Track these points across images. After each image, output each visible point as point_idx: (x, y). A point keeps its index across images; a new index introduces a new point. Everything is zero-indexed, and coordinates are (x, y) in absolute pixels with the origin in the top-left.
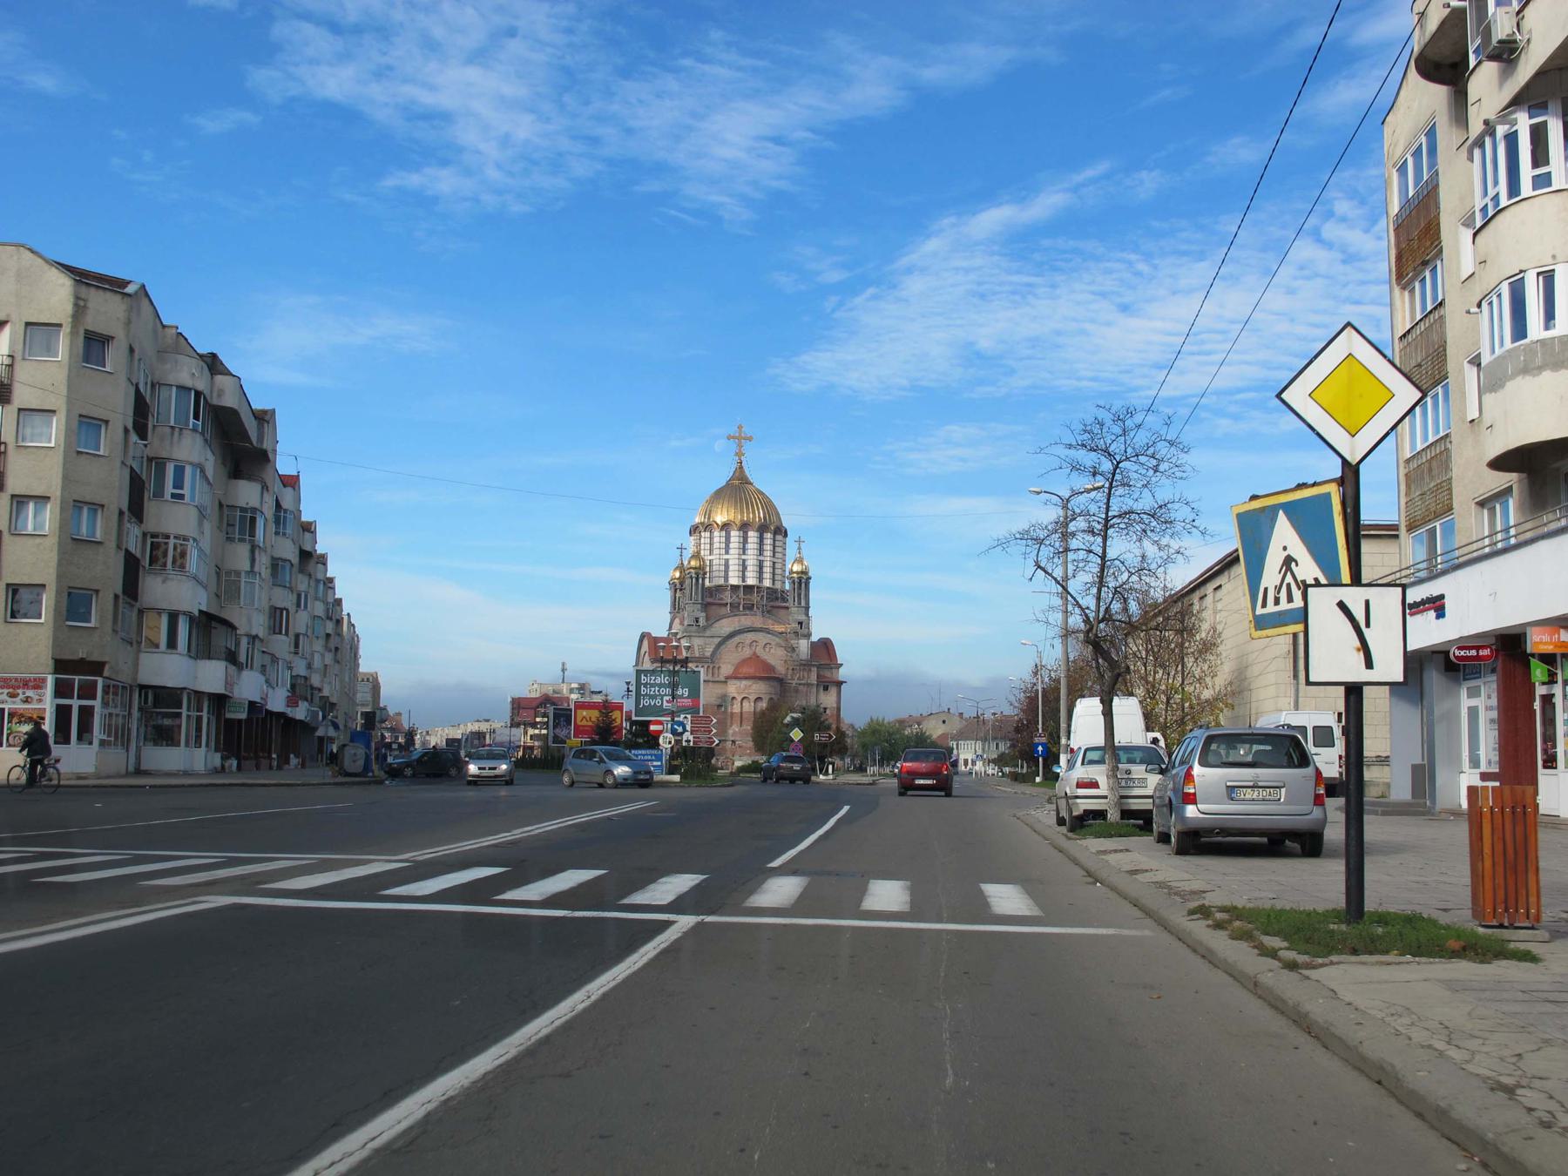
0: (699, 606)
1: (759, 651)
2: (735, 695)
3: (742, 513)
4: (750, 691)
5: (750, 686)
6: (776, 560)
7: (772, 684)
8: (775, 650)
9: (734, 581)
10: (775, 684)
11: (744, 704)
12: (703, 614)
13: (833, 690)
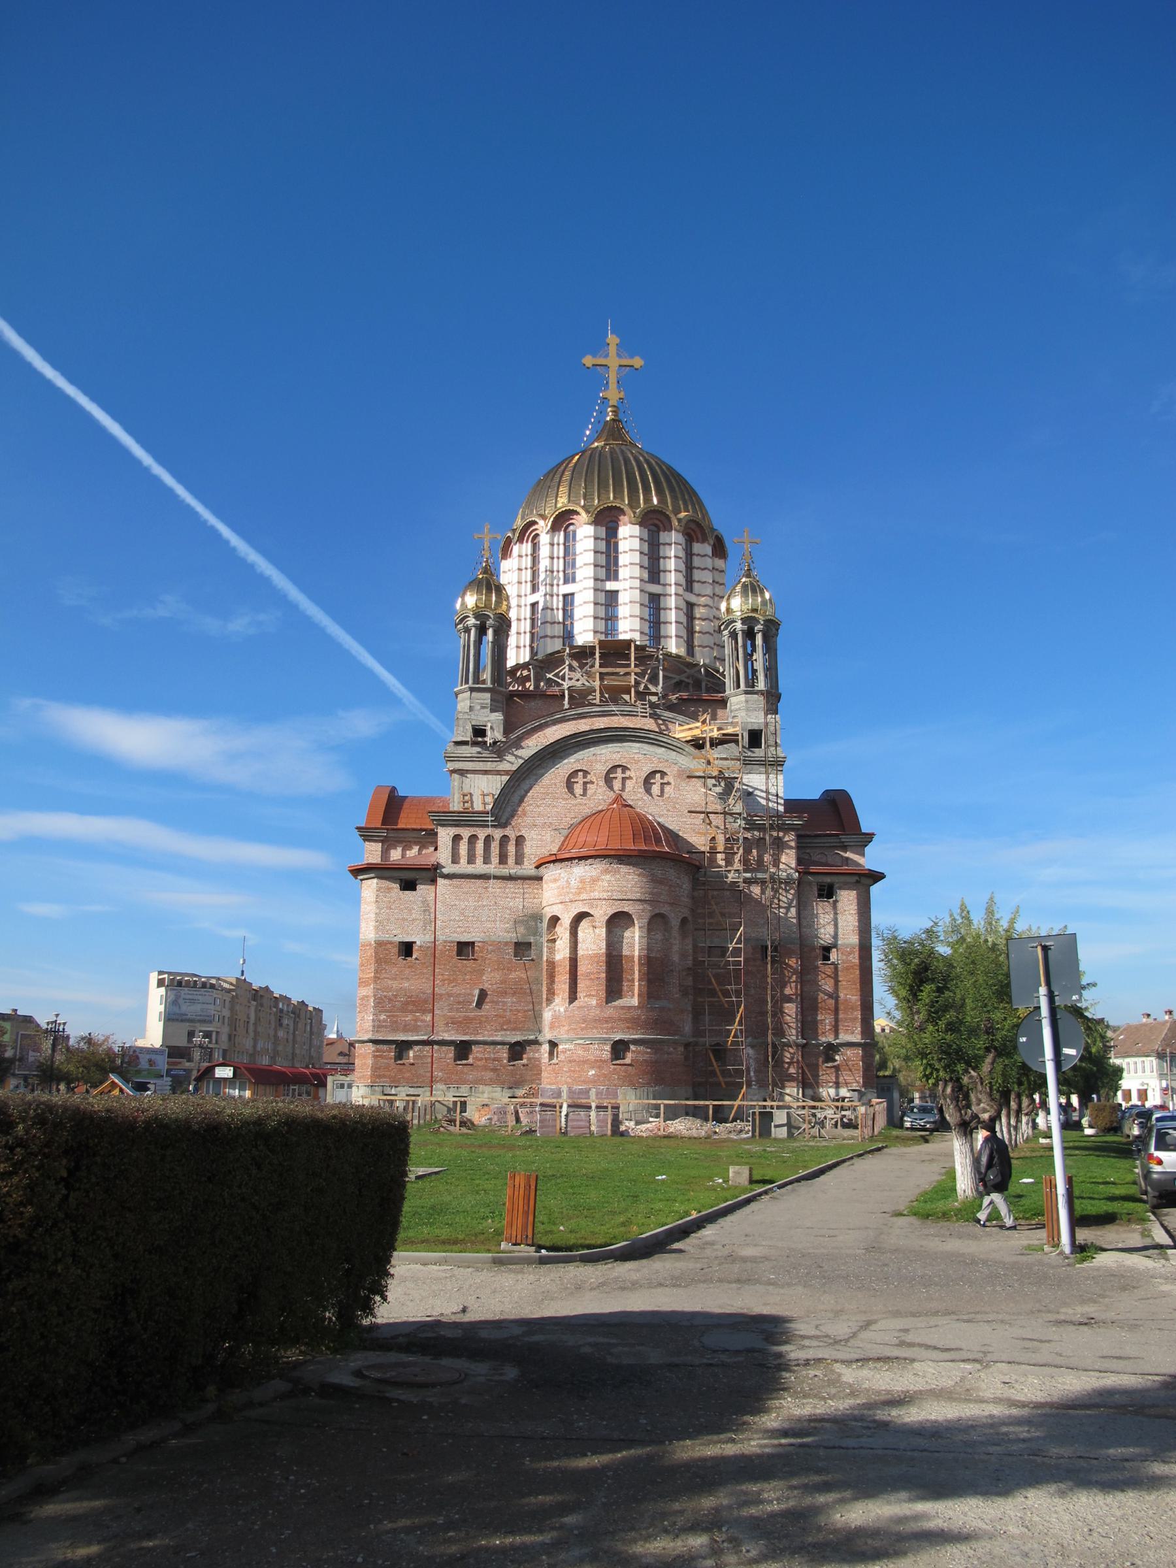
0: (488, 695)
1: (634, 793)
2: (556, 910)
3: (602, 486)
4: (596, 895)
5: (594, 880)
6: (693, 599)
7: (659, 873)
8: (677, 788)
9: (585, 633)
10: (672, 874)
11: (580, 934)
12: (498, 717)
13: (847, 899)
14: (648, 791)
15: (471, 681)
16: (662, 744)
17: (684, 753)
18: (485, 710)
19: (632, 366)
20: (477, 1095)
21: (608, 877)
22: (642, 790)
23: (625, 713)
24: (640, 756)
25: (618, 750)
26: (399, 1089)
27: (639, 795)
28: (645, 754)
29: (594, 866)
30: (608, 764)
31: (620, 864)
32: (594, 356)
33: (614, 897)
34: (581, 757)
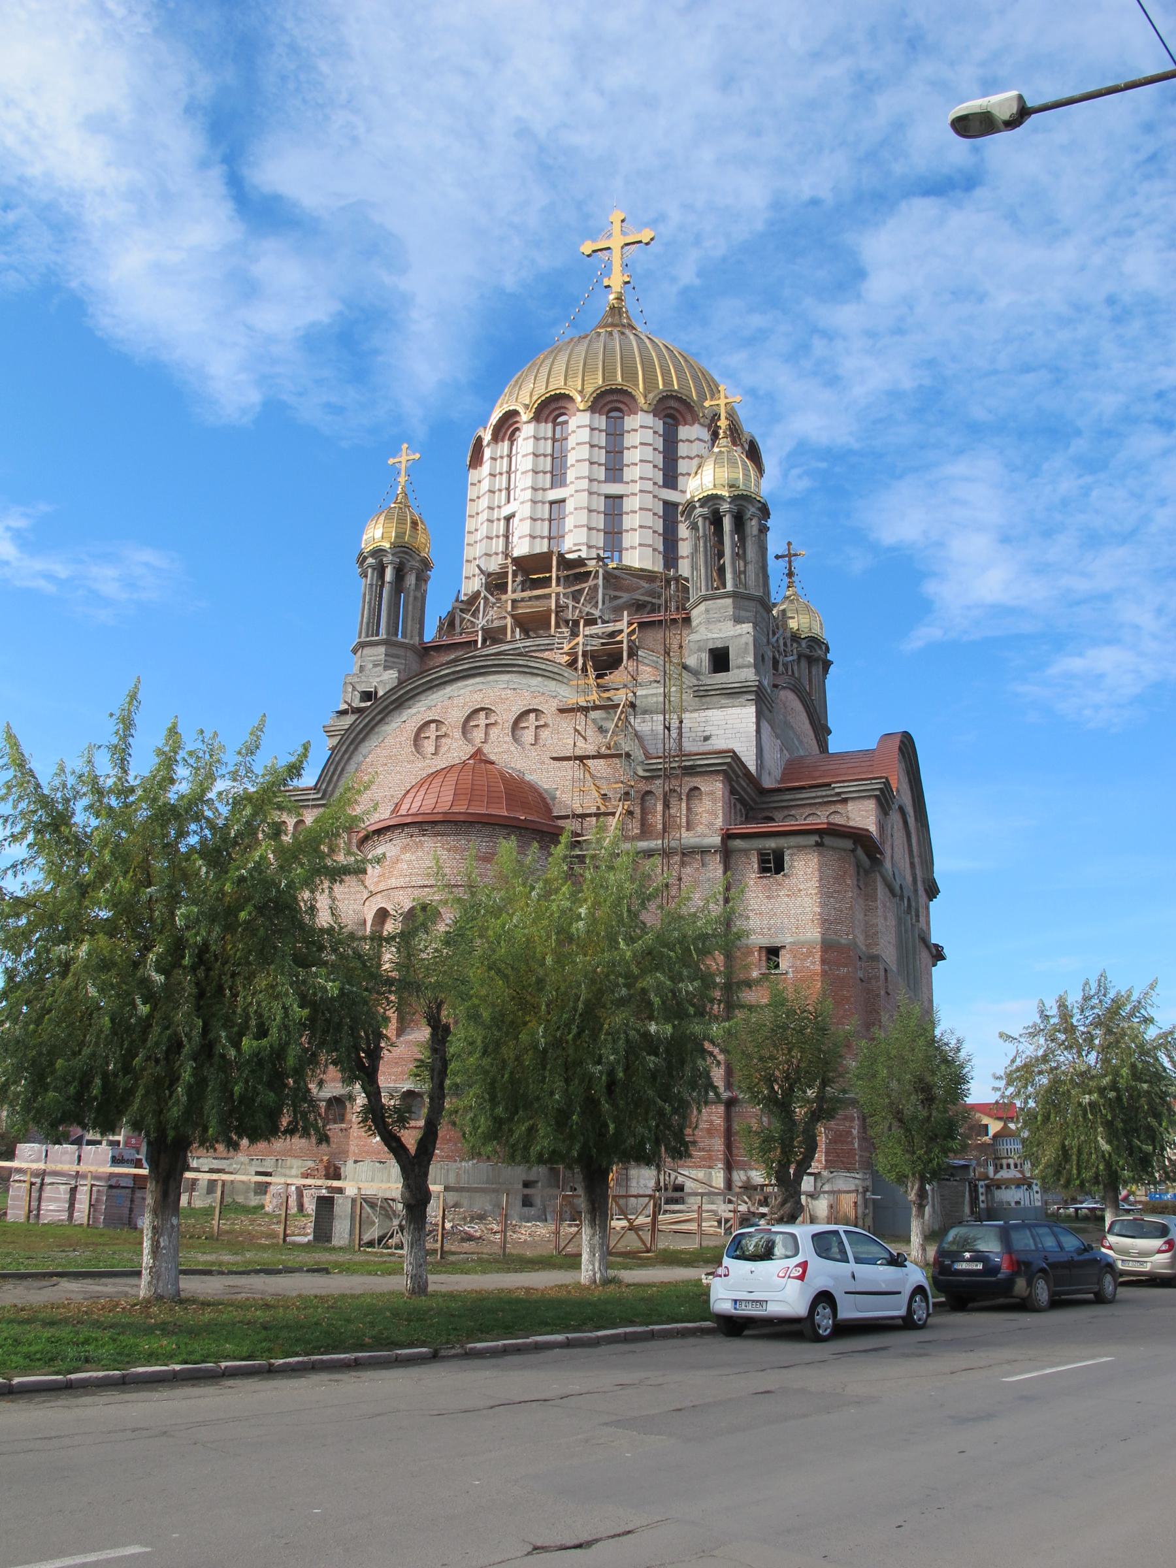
4: (393, 882)
14: (516, 739)
15: (363, 635)
16: (536, 671)
17: (565, 681)
18: (379, 668)
19: (640, 242)
20: (283, 1171)
21: (407, 856)
22: (509, 739)
23: (543, 648)
24: (509, 692)
25: (481, 687)
26: (201, 1160)
27: (505, 746)
28: (514, 689)
29: (394, 842)
30: (466, 708)
31: (424, 835)
32: (594, 240)
33: (413, 884)
34: (433, 703)
